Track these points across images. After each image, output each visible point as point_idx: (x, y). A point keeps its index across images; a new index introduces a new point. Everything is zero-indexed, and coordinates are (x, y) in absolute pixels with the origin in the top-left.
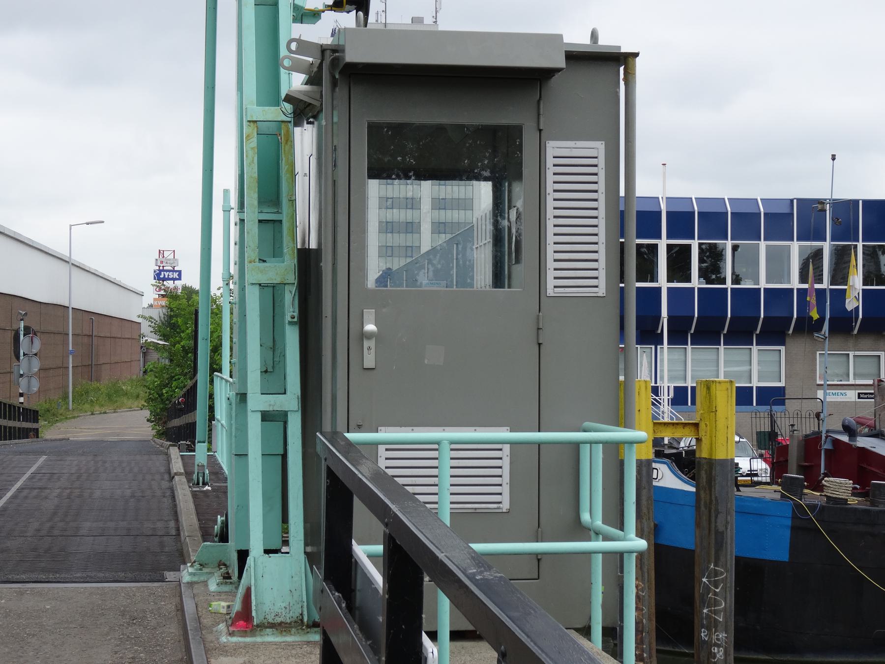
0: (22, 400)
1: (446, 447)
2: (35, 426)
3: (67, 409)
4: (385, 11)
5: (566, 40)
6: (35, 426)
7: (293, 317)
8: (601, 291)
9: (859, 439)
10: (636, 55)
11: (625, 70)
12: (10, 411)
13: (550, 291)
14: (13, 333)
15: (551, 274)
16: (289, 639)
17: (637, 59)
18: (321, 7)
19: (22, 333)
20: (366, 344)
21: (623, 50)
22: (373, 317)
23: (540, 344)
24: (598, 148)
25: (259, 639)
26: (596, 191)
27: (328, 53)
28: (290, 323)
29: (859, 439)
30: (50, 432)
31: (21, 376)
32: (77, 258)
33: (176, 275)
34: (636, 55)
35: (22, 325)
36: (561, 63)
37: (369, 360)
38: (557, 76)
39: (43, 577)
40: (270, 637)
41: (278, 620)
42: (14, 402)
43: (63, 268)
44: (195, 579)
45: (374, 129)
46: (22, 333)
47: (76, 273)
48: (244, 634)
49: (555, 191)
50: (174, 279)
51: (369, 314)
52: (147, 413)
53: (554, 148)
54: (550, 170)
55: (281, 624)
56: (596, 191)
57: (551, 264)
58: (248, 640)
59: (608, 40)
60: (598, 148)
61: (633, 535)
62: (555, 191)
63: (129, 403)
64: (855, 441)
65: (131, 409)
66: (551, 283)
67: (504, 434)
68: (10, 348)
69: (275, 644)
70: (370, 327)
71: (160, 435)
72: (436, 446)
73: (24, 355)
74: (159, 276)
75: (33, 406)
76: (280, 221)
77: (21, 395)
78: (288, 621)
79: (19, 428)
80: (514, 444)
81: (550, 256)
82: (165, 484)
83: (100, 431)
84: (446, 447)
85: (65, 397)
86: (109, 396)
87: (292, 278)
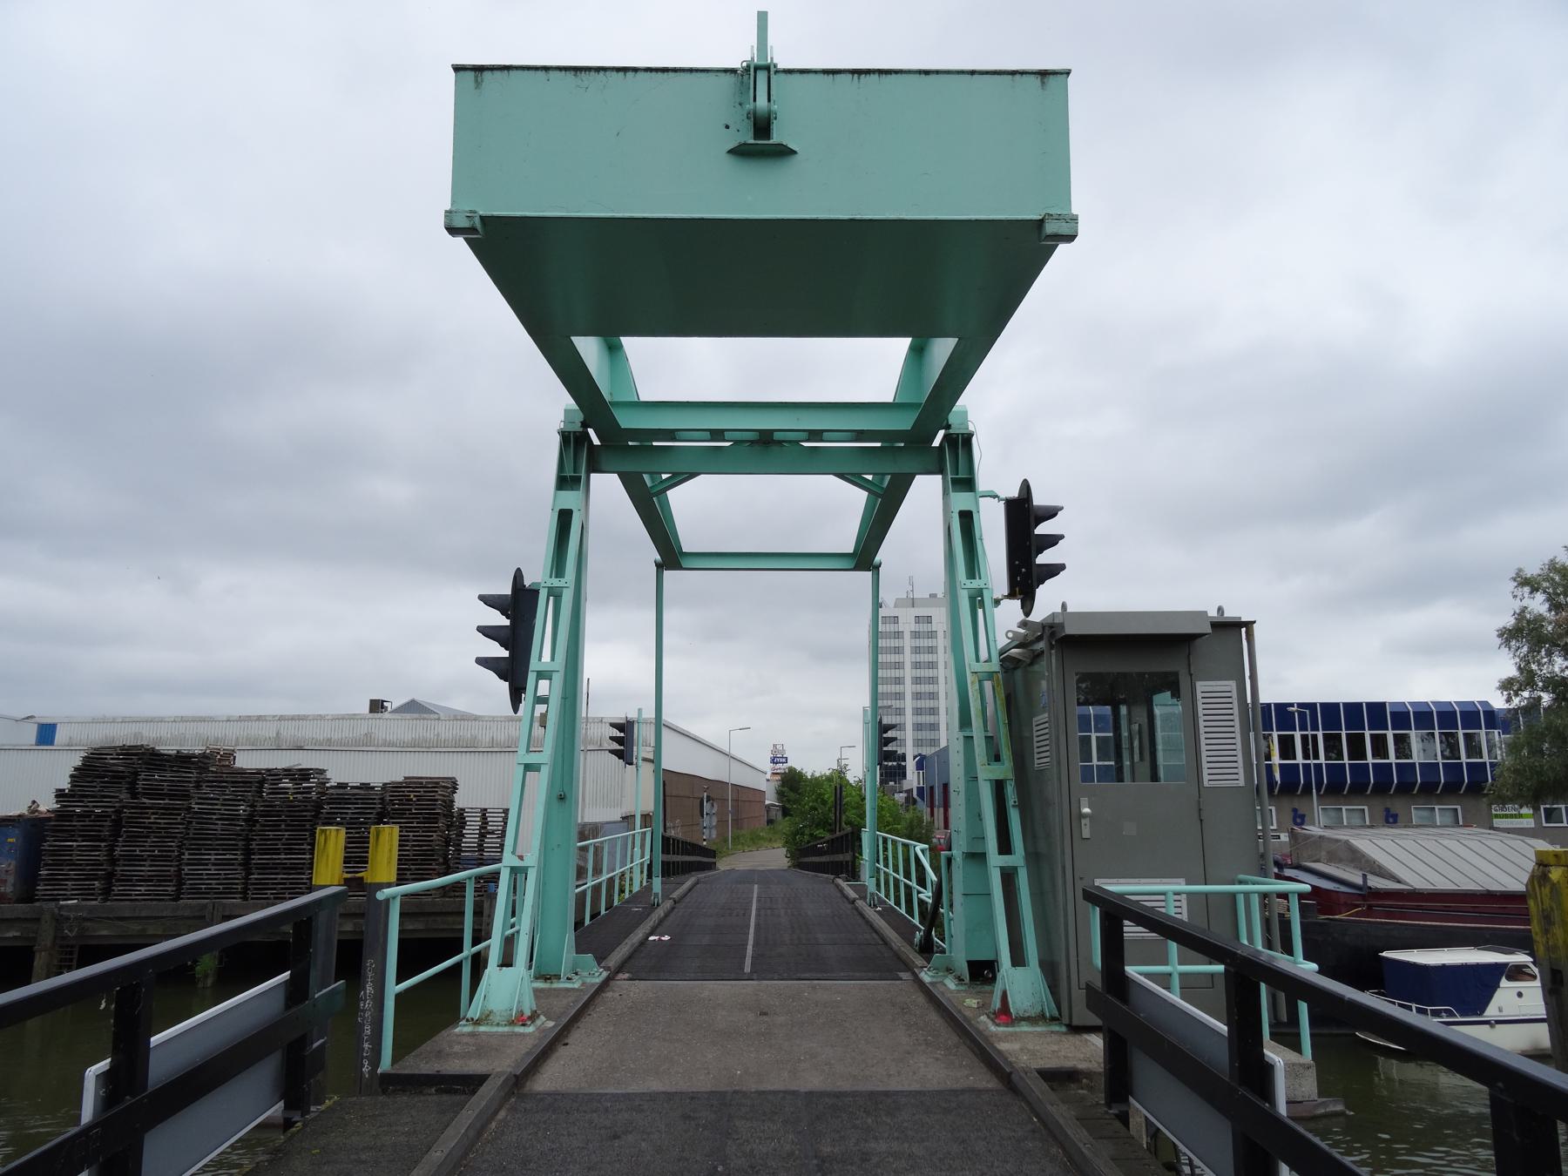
0: (705, 843)
1: (1171, 894)
2: (713, 860)
3: (728, 848)
4: (912, 591)
5: (1209, 615)
6: (713, 860)
7: (1015, 802)
8: (1241, 783)
9: (1285, 870)
10: (1254, 622)
11: (1247, 632)
12: (434, 818)
13: (1206, 784)
14: (699, 801)
15: (1205, 772)
16: (1038, 1029)
17: (1254, 625)
18: (1000, 597)
19: (705, 800)
20: (1083, 822)
21: (1243, 620)
22: (1087, 803)
23: (1201, 820)
24: (1232, 685)
25: (1017, 1029)
26: (1232, 715)
27: (1047, 628)
28: (1013, 806)
29: (1285, 870)
30: (723, 865)
31: (705, 828)
32: (734, 753)
33: (784, 760)
34: (1254, 622)
35: (705, 794)
36: (1209, 630)
37: (1086, 833)
38: (1199, 641)
39: (819, 976)
40: (1025, 1028)
41: (1027, 1015)
42: (700, 843)
43: (727, 758)
44: (934, 980)
45: (1083, 678)
46: (705, 800)
47: (734, 764)
48: (1007, 1025)
49: (1204, 715)
50: (783, 763)
51: (1084, 801)
52: (785, 850)
53: (1201, 686)
54: (1200, 701)
55: (1029, 1017)
56: (1232, 715)
57: (1205, 765)
58: (1010, 1029)
59: (1230, 614)
60: (1232, 685)
61: (1301, 959)
62: (1204, 715)
63: (766, 844)
64: (1283, 871)
65: (767, 848)
66: (1206, 777)
67: (1182, 886)
68: (697, 812)
69: (1030, 1033)
70: (1086, 810)
71: (795, 866)
72: (1162, 897)
73: (707, 814)
74: (773, 761)
75: (714, 848)
76: (972, 737)
77: (705, 840)
78: (1033, 1015)
79: (682, 862)
80: (1190, 894)
81: (1204, 759)
82: (849, 906)
83: (752, 863)
84: (1171, 894)
85: (726, 841)
86: (752, 839)
87: (1010, 775)
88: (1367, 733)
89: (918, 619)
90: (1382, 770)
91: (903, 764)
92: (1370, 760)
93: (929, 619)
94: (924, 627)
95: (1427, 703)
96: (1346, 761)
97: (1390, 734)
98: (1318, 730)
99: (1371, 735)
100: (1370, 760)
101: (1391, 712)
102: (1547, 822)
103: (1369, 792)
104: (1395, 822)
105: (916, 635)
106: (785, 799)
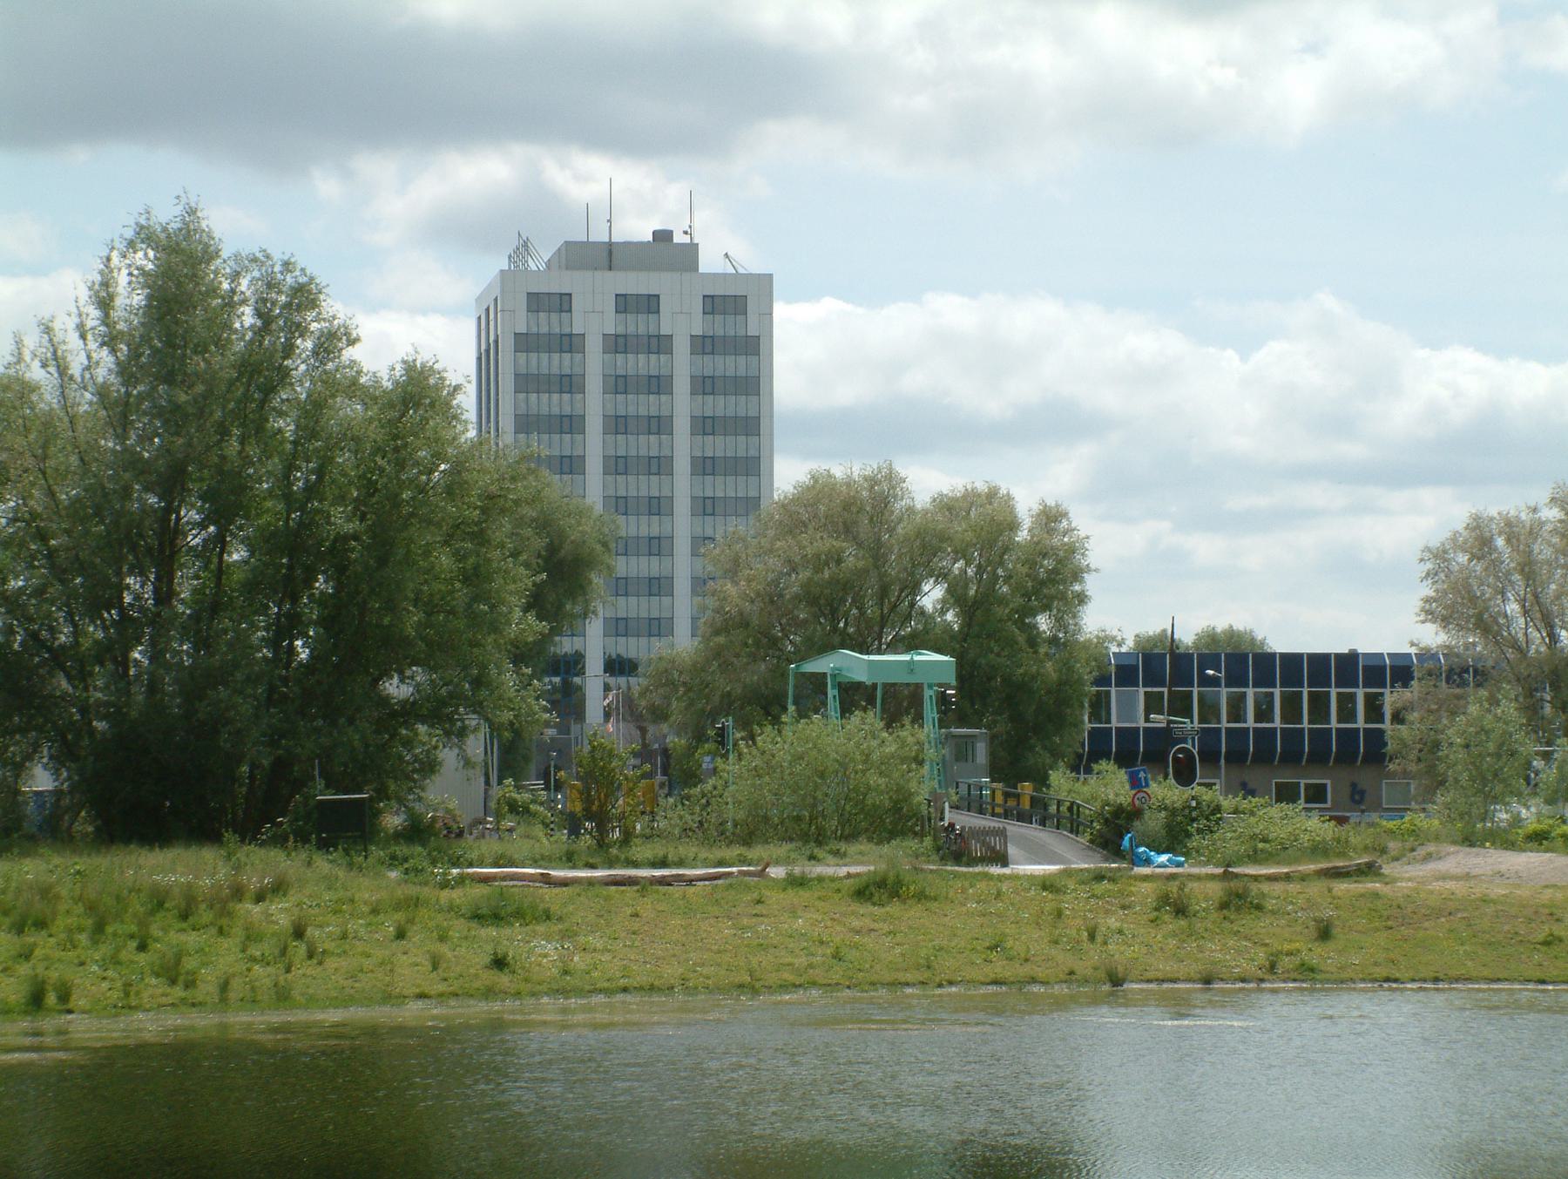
70: (311, 633)
88: (1334, 692)
89: (624, 303)
90: (1237, 736)
91: (577, 680)
92: (1334, 723)
93: (651, 304)
94: (637, 325)
95: (1382, 654)
96: (1306, 725)
97: (1360, 693)
98: (1275, 687)
99: (1339, 694)
100: (1224, 724)
101: (1363, 666)
102: (1325, 786)
103: (1248, 763)
104: (1360, 802)
105: (617, 344)
106: (985, 679)
